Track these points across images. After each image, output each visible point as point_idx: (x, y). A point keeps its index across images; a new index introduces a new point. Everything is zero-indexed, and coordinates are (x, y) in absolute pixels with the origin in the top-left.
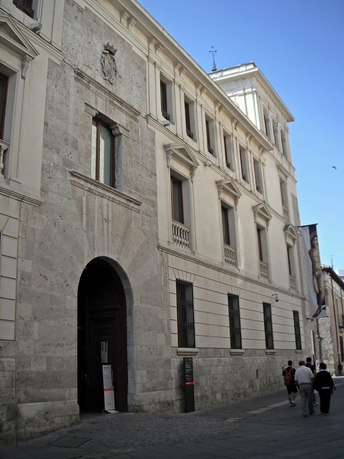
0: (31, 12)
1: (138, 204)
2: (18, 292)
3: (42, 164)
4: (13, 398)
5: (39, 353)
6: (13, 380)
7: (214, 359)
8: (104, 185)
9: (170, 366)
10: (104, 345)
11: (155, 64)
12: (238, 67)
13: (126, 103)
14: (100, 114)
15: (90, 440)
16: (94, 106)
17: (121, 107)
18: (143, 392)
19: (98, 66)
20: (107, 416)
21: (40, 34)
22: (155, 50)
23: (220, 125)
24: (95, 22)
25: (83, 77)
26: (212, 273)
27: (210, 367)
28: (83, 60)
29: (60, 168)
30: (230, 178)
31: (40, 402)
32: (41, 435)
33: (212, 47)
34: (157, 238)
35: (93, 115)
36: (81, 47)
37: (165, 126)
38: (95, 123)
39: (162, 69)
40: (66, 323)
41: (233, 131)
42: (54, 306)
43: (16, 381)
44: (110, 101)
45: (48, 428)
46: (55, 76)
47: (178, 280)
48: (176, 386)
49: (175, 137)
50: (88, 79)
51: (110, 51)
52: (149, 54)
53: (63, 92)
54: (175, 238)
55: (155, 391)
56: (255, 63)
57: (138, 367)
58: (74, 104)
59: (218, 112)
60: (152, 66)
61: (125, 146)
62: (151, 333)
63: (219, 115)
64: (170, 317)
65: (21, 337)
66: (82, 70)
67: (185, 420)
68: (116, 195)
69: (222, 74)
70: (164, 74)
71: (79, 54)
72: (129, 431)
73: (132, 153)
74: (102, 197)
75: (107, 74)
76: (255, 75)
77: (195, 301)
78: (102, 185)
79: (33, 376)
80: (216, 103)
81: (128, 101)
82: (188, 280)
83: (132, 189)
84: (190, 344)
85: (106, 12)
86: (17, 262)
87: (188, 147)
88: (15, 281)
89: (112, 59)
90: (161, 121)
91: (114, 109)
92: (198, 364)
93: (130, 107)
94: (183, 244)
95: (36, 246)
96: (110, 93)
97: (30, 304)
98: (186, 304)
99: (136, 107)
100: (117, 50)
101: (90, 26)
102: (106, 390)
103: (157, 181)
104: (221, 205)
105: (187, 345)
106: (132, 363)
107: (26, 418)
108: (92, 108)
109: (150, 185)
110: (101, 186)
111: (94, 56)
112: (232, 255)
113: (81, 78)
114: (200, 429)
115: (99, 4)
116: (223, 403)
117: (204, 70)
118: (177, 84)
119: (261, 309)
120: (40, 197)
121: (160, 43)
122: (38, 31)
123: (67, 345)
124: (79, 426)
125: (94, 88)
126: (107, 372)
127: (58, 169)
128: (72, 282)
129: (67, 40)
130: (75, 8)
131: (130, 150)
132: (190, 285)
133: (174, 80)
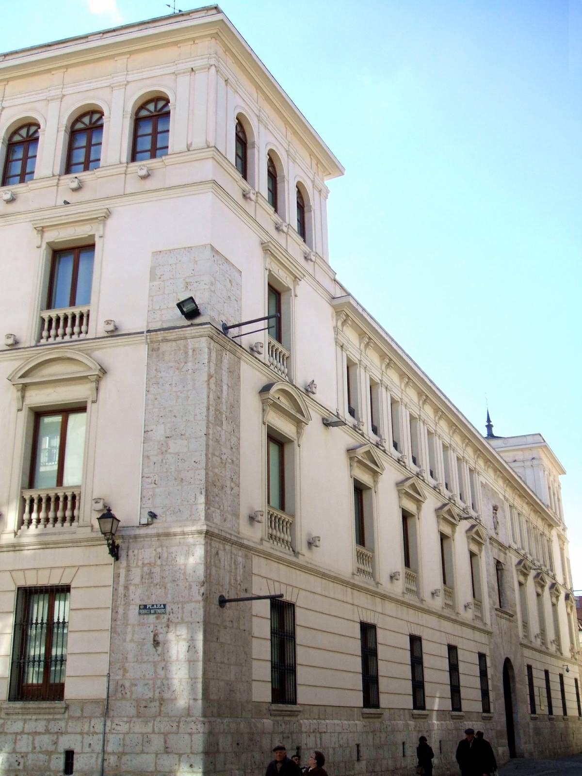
68: (502, 612)
98: (284, 636)
119: (358, 634)
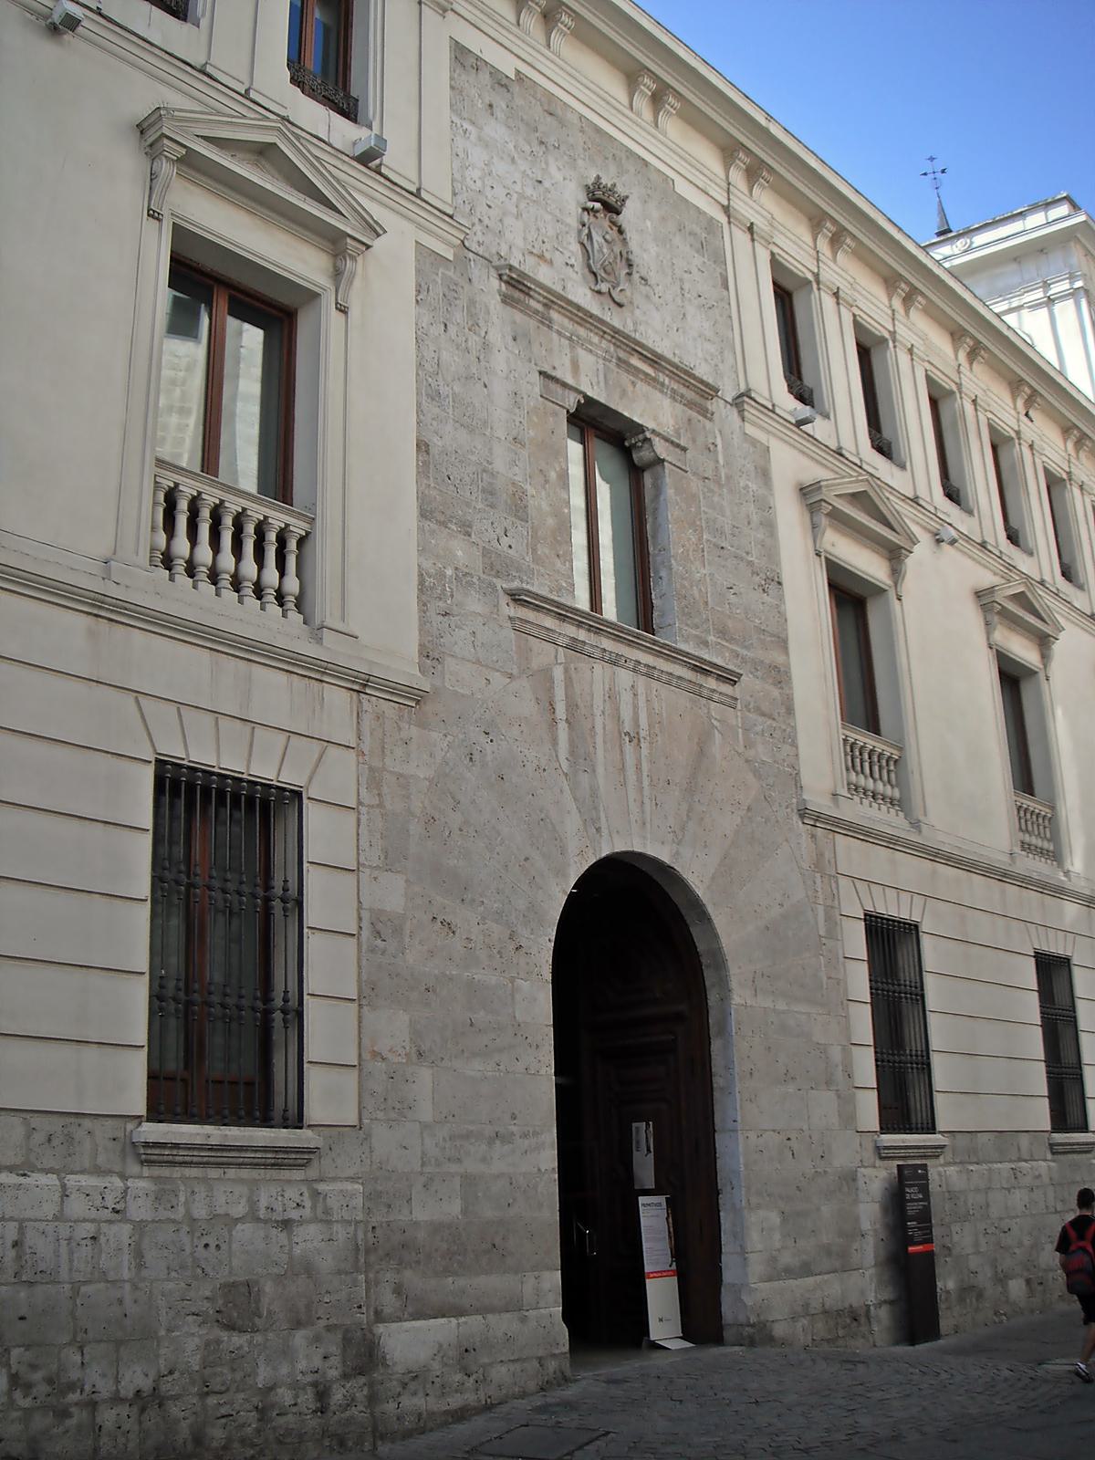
0: (349, 104)
1: (730, 678)
2: (364, 977)
3: (419, 571)
4: (360, 1307)
5: (438, 1164)
6: (357, 1249)
7: (999, 1169)
8: (616, 625)
9: (857, 1195)
10: (643, 1132)
11: (751, 229)
12: (1021, 215)
13: (549, 288)
14: (590, 402)
15: (603, 1435)
16: (570, 381)
17: (653, 375)
18: (770, 1280)
19: (570, 251)
20: (657, 1359)
21: (384, 170)
22: (749, 187)
23: (976, 410)
24: (551, 114)
25: (527, 292)
26: (979, 889)
27: (987, 1193)
28: (525, 239)
29: (477, 583)
30: (1024, 578)
31: (443, 1316)
32: (450, 1420)
33: (932, 159)
34: (796, 785)
35: (567, 406)
36: (515, 196)
37: (800, 423)
38: (576, 431)
39: (776, 245)
40: (520, 1066)
41: (1019, 426)
42: (481, 1016)
43: (367, 1252)
44: (619, 359)
45: (470, 1398)
46: (441, 295)
47: (871, 916)
48: (875, 1257)
49: (836, 458)
50: (545, 298)
51: (605, 202)
52: (729, 200)
53: (470, 344)
54: (863, 785)
55: (810, 1273)
56: (1074, 197)
57: (754, 1200)
58: (507, 378)
59: (967, 366)
60: (742, 238)
61: (678, 498)
62: (791, 1089)
63: (971, 376)
64: (849, 1038)
65: (380, 1115)
66: (522, 268)
67: (911, 1370)
68: (659, 654)
69: (972, 243)
70: (783, 258)
71: (509, 221)
72: (728, 1405)
73: (701, 519)
74: (614, 664)
75: (603, 275)
76: (1075, 236)
77: (930, 983)
78: (610, 628)
79: (421, 1235)
80: (959, 339)
81: (674, 354)
82: (904, 915)
83: (708, 631)
84: (919, 1121)
85: (585, 81)
86: (358, 882)
87: (879, 486)
88: (354, 940)
89: (615, 228)
90: (785, 411)
91: (634, 384)
92: (947, 1185)
93: (683, 375)
94: (883, 799)
95: (415, 828)
96: (616, 336)
97: (405, 1011)
99: (703, 371)
100: (627, 197)
101: (536, 130)
102: (652, 1275)
103: (784, 603)
104: (828, 579)
105: (910, 1124)
106: (733, 1189)
107: (400, 1369)
108: (565, 385)
109: (763, 618)
110: (609, 630)
111: (558, 221)
112: (1041, 827)
113: (522, 296)
114: (958, 1398)
115: (559, 57)
116: (1032, 1311)
117: (910, 237)
118: (828, 288)
120: (419, 674)
121: (763, 161)
122: (377, 161)
123: (525, 1136)
124: (570, 1392)
125: (566, 321)
126: (653, 1217)
127: (471, 584)
128: (532, 936)
129: (468, 179)
130: (485, 77)
131: (693, 510)
132: (912, 929)
133: (817, 276)
